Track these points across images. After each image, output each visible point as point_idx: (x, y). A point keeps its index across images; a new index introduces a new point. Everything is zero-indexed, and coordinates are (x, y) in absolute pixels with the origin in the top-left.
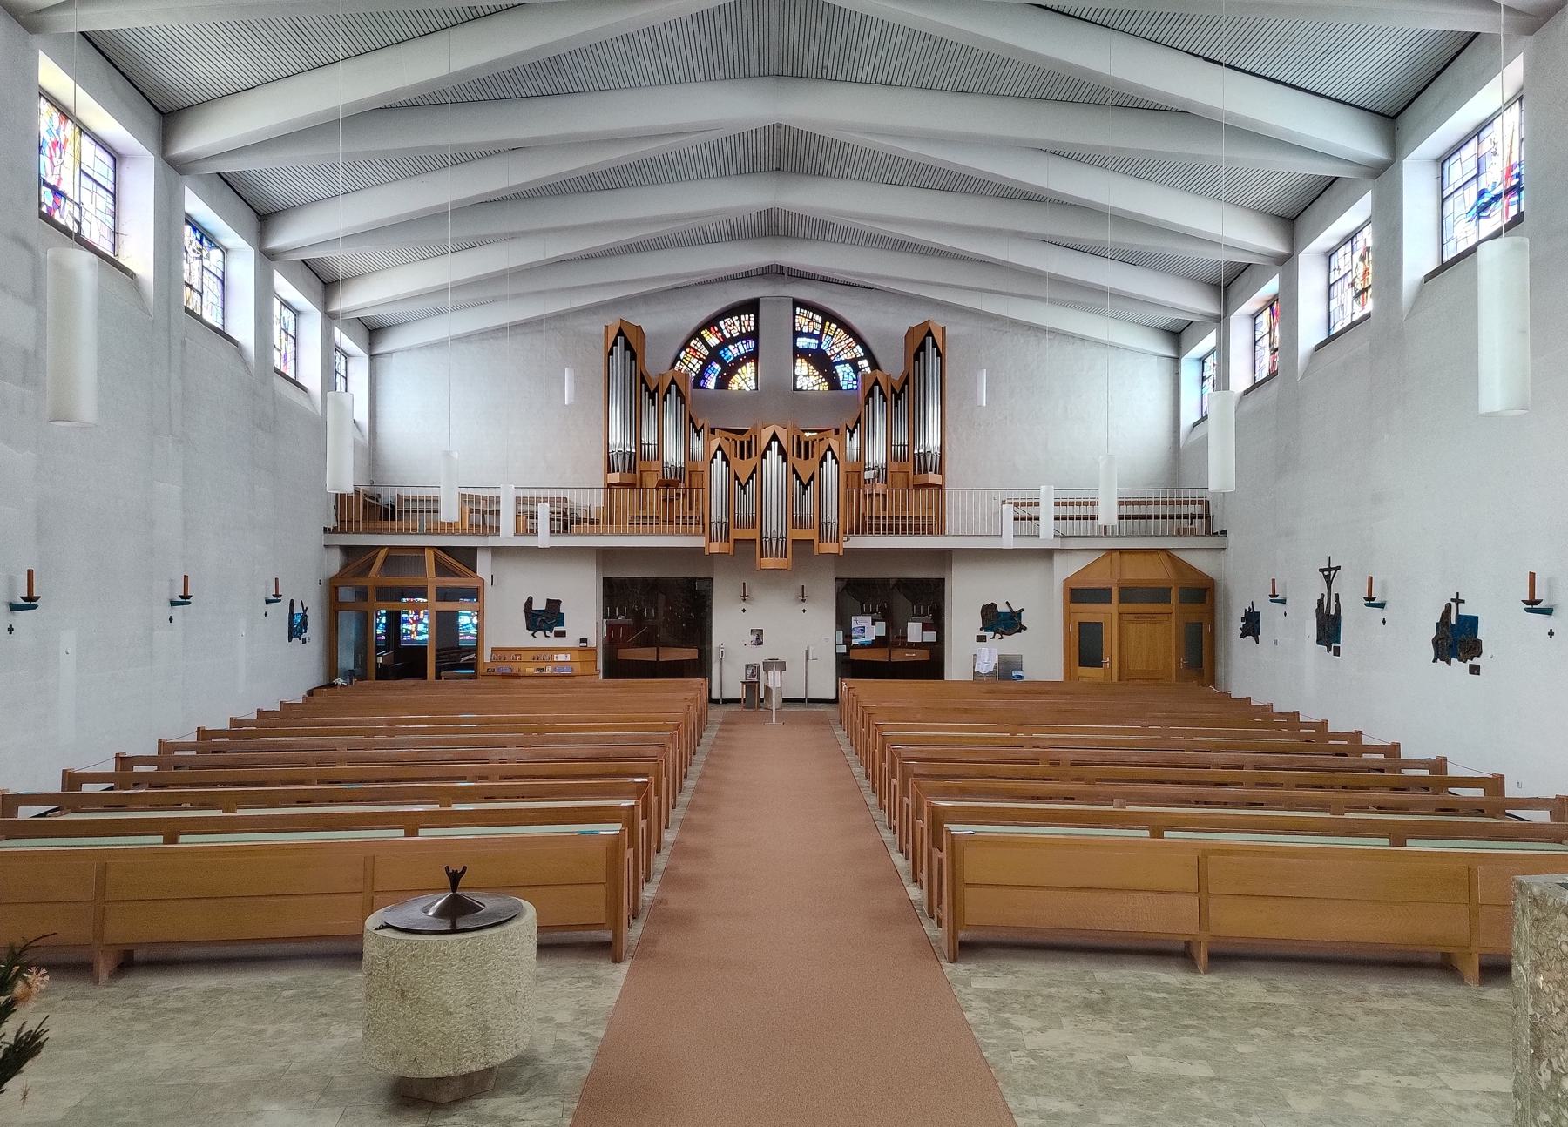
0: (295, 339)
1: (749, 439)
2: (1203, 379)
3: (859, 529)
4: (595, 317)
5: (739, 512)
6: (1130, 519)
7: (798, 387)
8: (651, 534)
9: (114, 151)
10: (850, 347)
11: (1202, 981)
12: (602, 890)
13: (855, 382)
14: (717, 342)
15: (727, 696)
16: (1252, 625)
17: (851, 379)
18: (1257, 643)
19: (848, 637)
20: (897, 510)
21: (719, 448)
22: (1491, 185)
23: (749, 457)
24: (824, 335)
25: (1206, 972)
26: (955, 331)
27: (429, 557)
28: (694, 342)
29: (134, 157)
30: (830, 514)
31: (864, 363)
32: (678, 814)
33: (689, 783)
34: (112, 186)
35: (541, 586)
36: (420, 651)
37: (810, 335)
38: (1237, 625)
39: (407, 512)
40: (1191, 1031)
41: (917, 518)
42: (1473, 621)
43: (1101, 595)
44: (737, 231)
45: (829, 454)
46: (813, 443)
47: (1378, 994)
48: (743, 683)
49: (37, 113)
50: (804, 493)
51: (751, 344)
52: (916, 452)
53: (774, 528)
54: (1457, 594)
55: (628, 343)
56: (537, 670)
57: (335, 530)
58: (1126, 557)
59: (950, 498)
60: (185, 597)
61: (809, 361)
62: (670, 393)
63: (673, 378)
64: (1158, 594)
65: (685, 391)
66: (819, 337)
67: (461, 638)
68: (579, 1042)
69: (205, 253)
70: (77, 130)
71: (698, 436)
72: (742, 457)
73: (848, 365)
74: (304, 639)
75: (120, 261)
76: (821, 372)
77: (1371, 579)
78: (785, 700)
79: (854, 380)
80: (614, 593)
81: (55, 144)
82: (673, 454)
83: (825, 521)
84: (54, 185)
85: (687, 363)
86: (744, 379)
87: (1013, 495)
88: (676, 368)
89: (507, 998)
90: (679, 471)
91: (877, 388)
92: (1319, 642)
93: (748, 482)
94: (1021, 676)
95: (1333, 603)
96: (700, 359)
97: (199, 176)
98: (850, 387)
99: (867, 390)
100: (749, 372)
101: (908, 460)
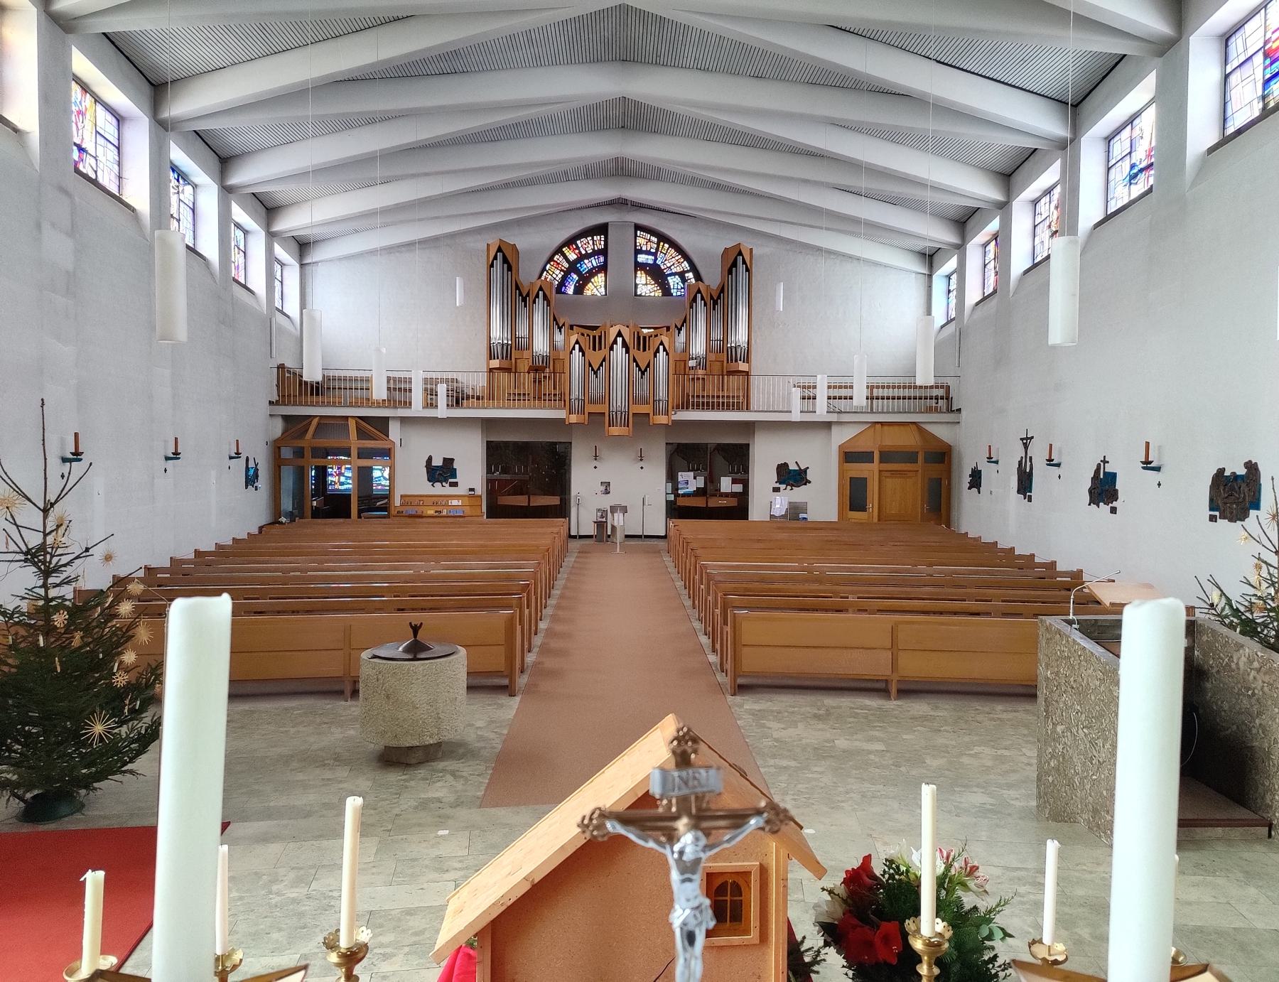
0: (245, 253)
2: (949, 291)
3: (685, 405)
4: (479, 236)
5: (592, 391)
6: (916, 399)
7: (639, 293)
8: (524, 408)
9: (119, 115)
11: (892, 704)
12: (502, 648)
13: (683, 290)
14: (575, 257)
15: (582, 533)
16: (976, 480)
18: (979, 493)
19: (675, 490)
21: (577, 342)
22: (1139, 160)
23: (600, 349)
24: (659, 252)
25: (895, 700)
26: (761, 250)
27: (352, 424)
28: (557, 257)
29: (131, 119)
30: (662, 393)
31: (690, 275)
32: (548, 611)
33: (556, 592)
34: (117, 141)
35: (439, 447)
36: (344, 498)
37: (648, 253)
38: (967, 480)
39: (334, 388)
40: (877, 728)
41: (728, 397)
42: (1114, 476)
43: (866, 457)
44: (592, 172)
46: (649, 337)
47: (1001, 710)
49: (69, 89)
50: (642, 378)
51: (602, 259)
52: (729, 345)
53: (619, 404)
54: (1105, 457)
55: (506, 257)
56: (436, 512)
57: (277, 403)
58: (886, 428)
59: (754, 381)
60: (176, 454)
61: (647, 273)
63: (541, 286)
64: (910, 457)
65: (550, 295)
66: (655, 254)
67: (374, 488)
68: (492, 736)
69: (181, 189)
70: (93, 100)
71: (560, 331)
72: (594, 349)
73: (677, 277)
74: (256, 487)
75: (124, 199)
76: (656, 282)
77: (1051, 445)
78: (627, 536)
80: (495, 453)
81: (79, 112)
82: (540, 345)
83: (658, 399)
84: (79, 145)
85: (551, 273)
86: (597, 286)
87: (802, 380)
88: (543, 278)
89: (451, 702)
90: (546, 359)
91: (699, 296)
92: (1019, 492)
93: (599, 369)
94: (805, 518)
95: (1028, 464)
96: (561, 270)
97: (180, 132)
98: (679, 294)
100: (600, 281)
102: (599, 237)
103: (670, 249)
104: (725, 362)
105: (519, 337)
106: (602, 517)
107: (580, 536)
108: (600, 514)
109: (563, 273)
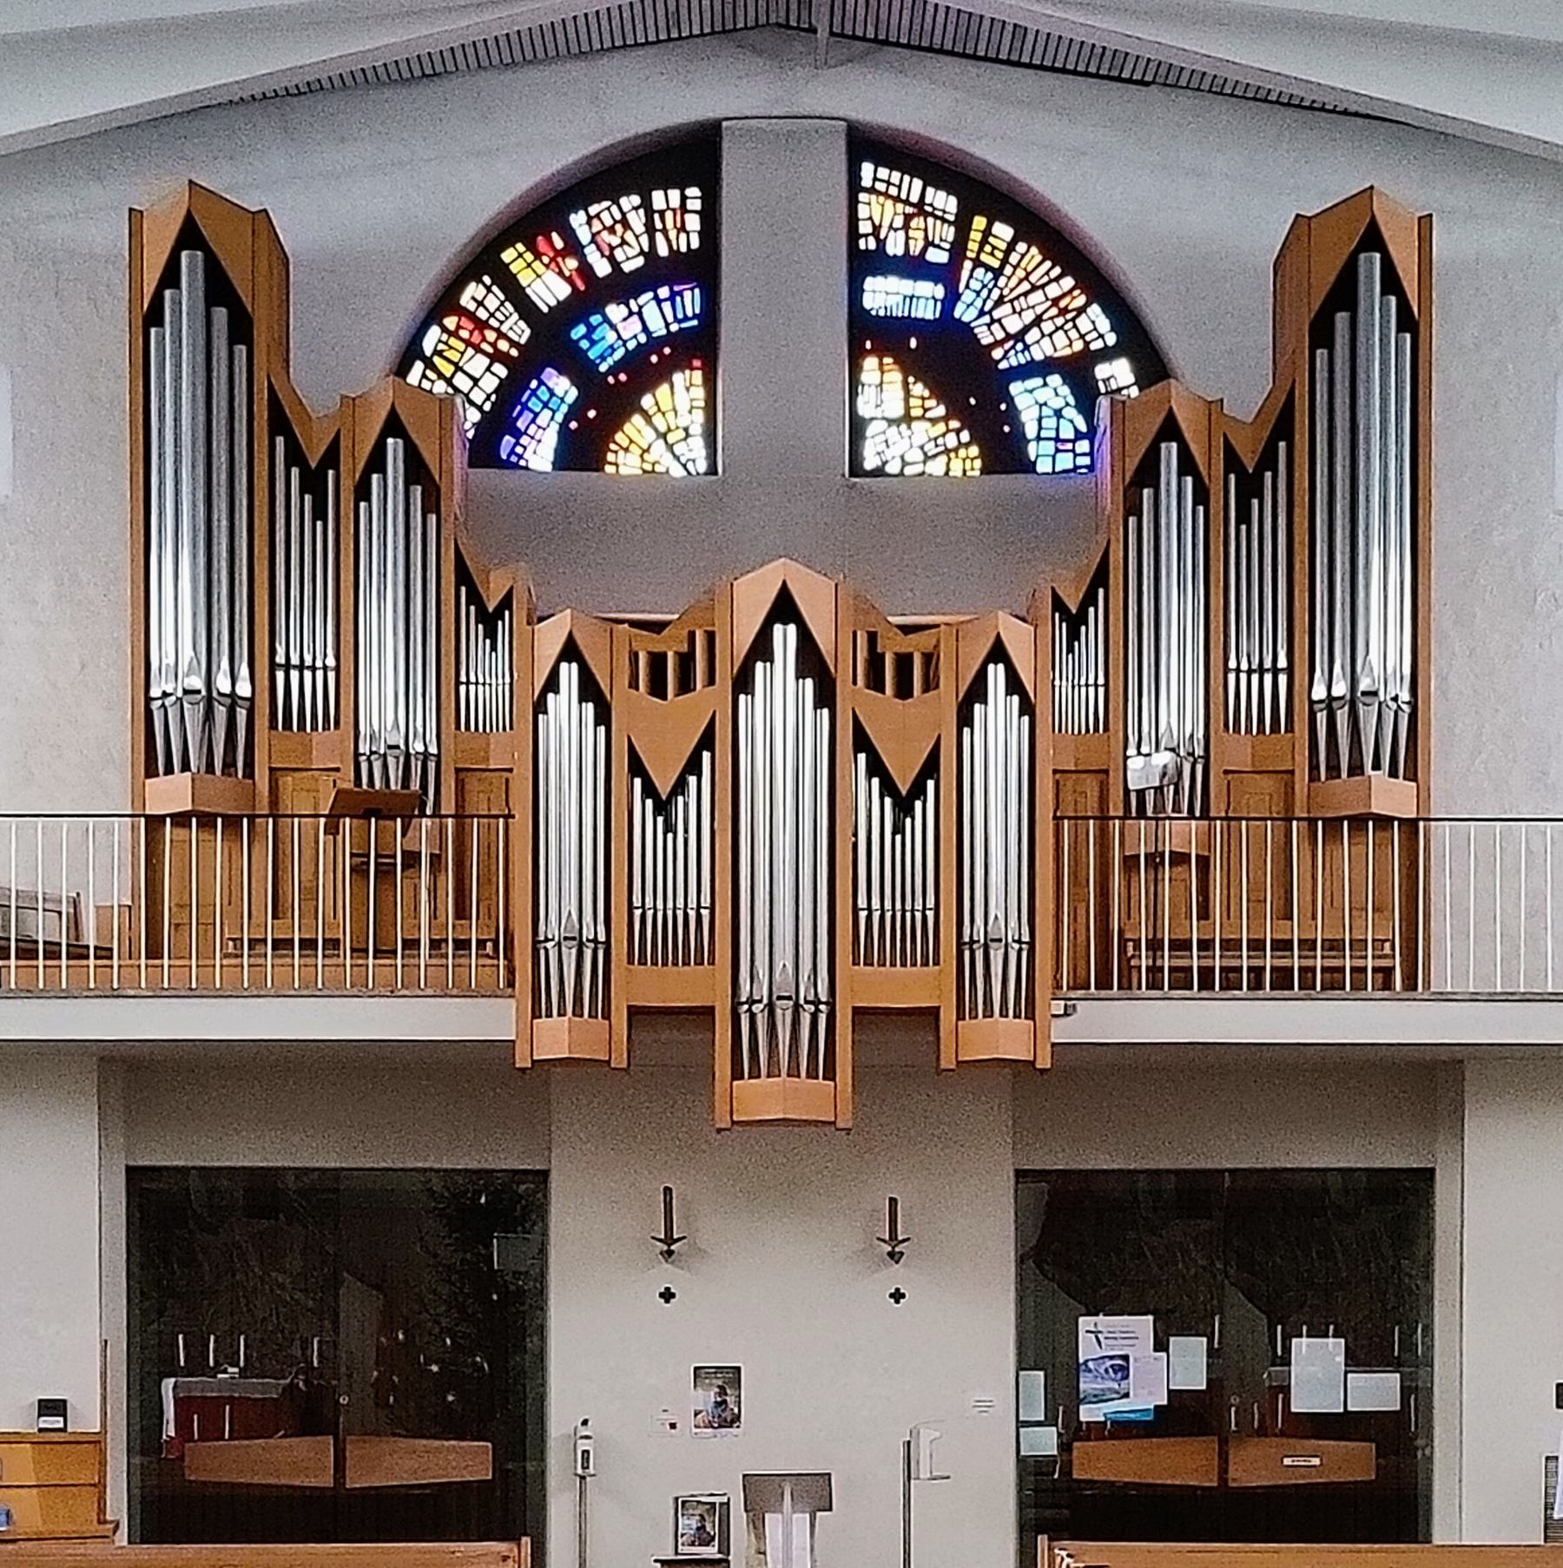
1: (685, 648)
4: (95, 188)
7: (870, 463)
10: (1063, 312)
13: (1083, 446)
14: (564, 291)
17: (1067, 432)
20: (1256, 915)
21: (570, 652)
23: (685, 685)
24: (968, 265)
28: (472, 291)
31: (1118, 373)
37: (913, 266)
45: (996, 674)
50: (898, 829)
51: (691, 300)
52: (1319, 692)
53: (784, 959)
59: (1441, 838)
61: (911, 366)
62: (382, 470)
63: (393, 415)
66: (947, 275)
71: (491, 634)
73: (1055, 380)
76: (956, 409)
79: (1079, 436)
85: (448, 370)
91: (1169, 452)
93: (680, 787)
96: (497, 357)
98: (1065, 461)
99: (1132, 464)
100: (683, 406)
101: (1290, 728)
102: (674, 195)
103: (1021, 247)
104: (1302, 775)
105: (287, 667)
108: (694, 1523)
109: (501, 370)
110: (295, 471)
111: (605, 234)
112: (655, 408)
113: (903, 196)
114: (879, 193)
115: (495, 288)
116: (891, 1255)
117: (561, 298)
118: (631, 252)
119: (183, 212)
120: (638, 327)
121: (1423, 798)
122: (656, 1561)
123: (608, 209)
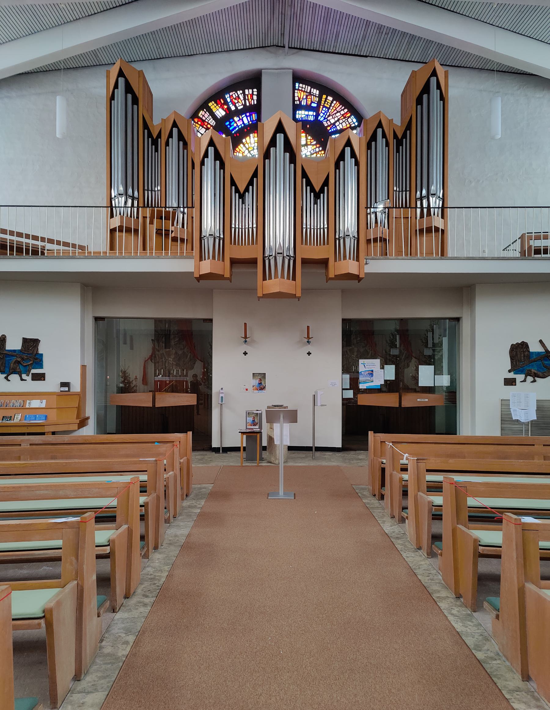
10: (345, 118)
14: (223, 113)
15: (226, 445)
19: (354, 384)
21: (211, 143)
24: (321, 107)
37: (308, 108)
48: (243, 433)
51: (254, 117)
63: (174, 122)
66: (316, 110)
78: (290, 448)
91: (380, 131)
93: (247, 190)
106: (254, 423)
107: (223, 448)
108: (251, 419)
110: (150, 139)
111: (234, 100)
112: (246, 142)
113: (306, 91)
114: (300, 90)
115: (207, 112)
116: (308, 342)
117: (223, 115)
118: (240, 104)
119: (119, 67)
120: (242, 123)
121: (446, 224)
122: (239, 432)
123: (235, 94)
